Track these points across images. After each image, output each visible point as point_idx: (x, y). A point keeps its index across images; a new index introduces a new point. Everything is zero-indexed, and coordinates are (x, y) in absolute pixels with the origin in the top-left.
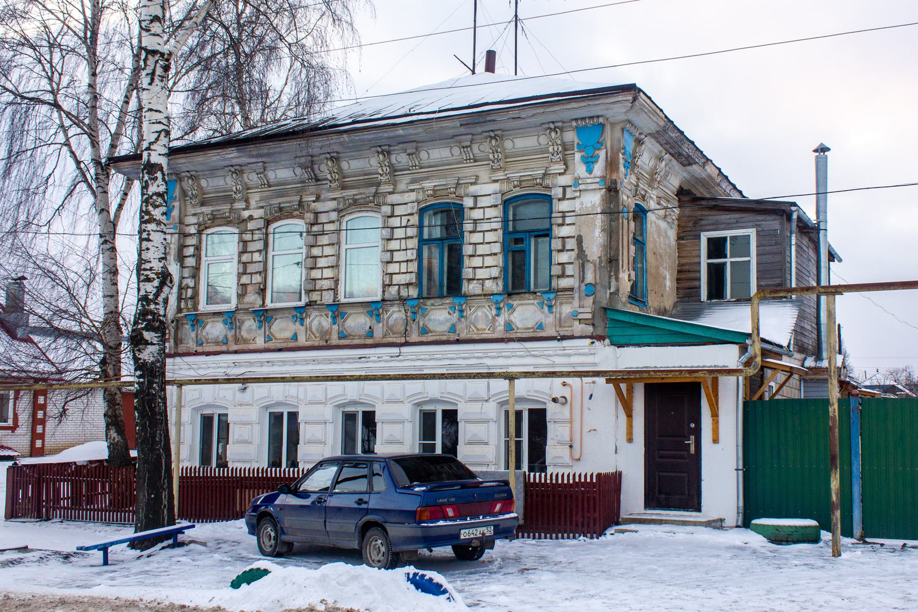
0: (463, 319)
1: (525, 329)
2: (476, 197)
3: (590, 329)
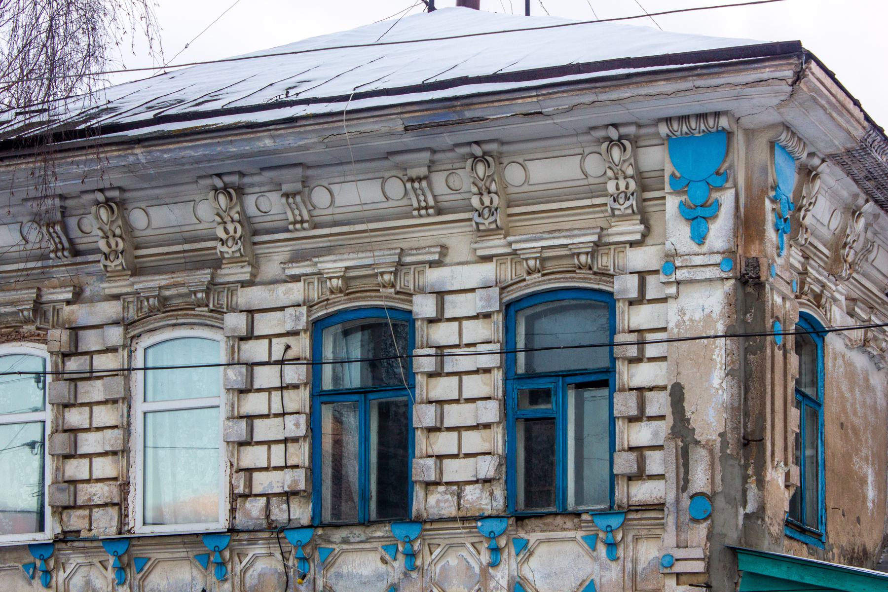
0: (414, 575)
2: (441, 295)
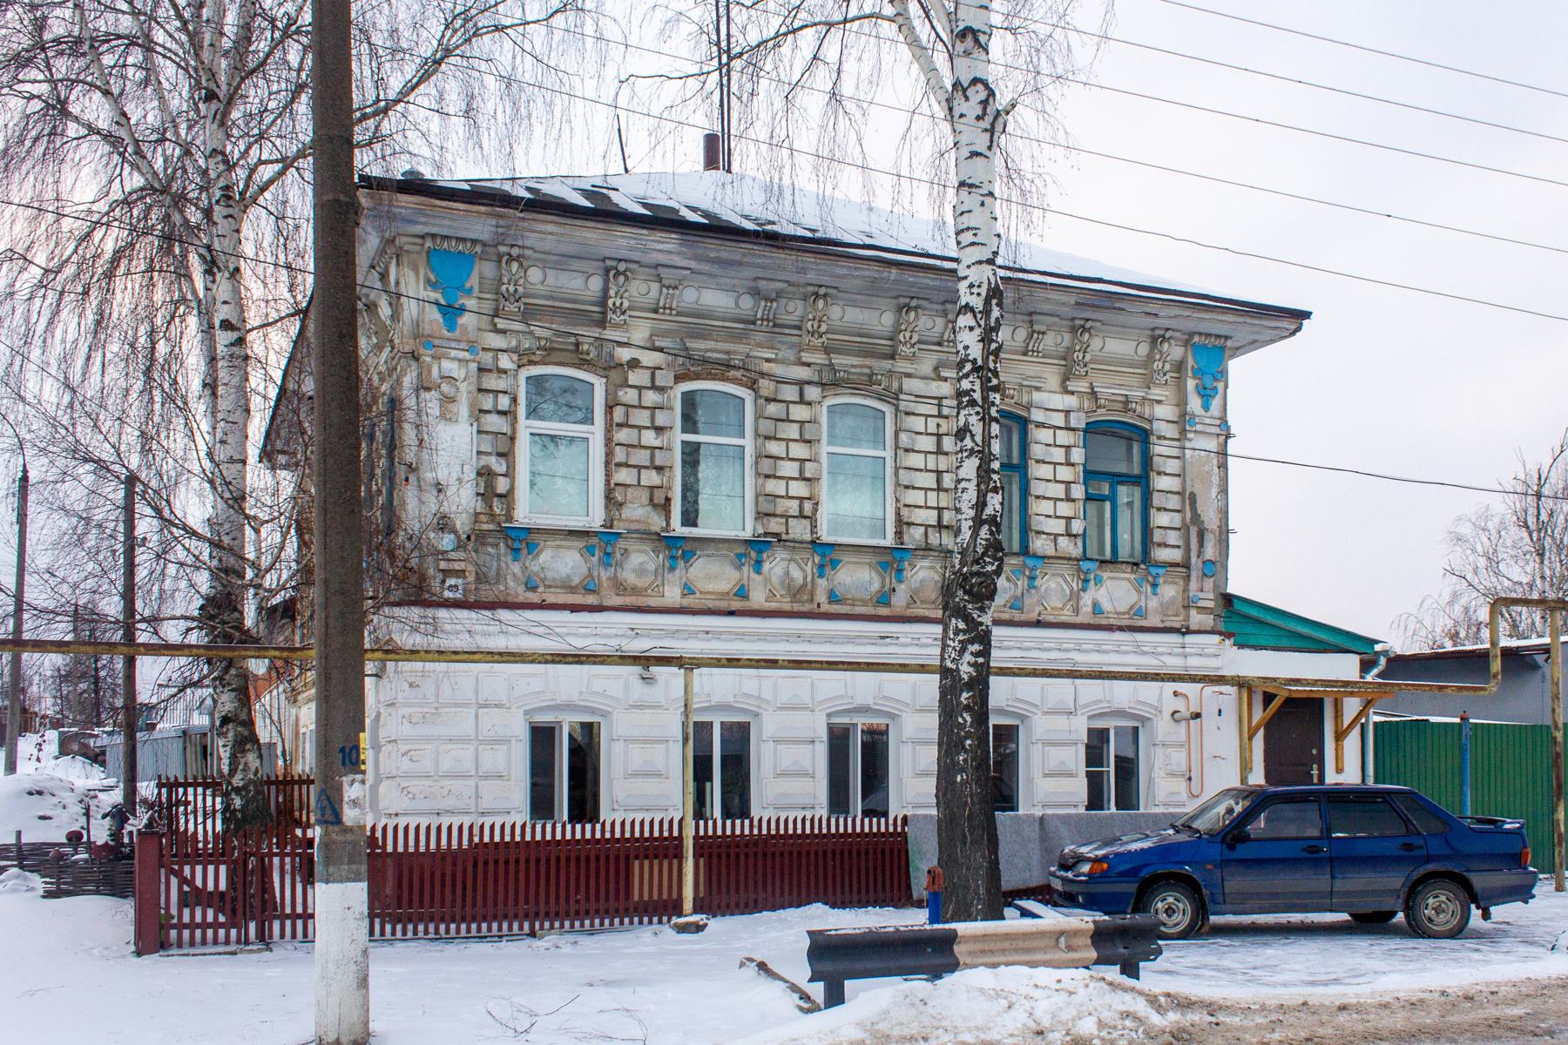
0: (1033, 591)
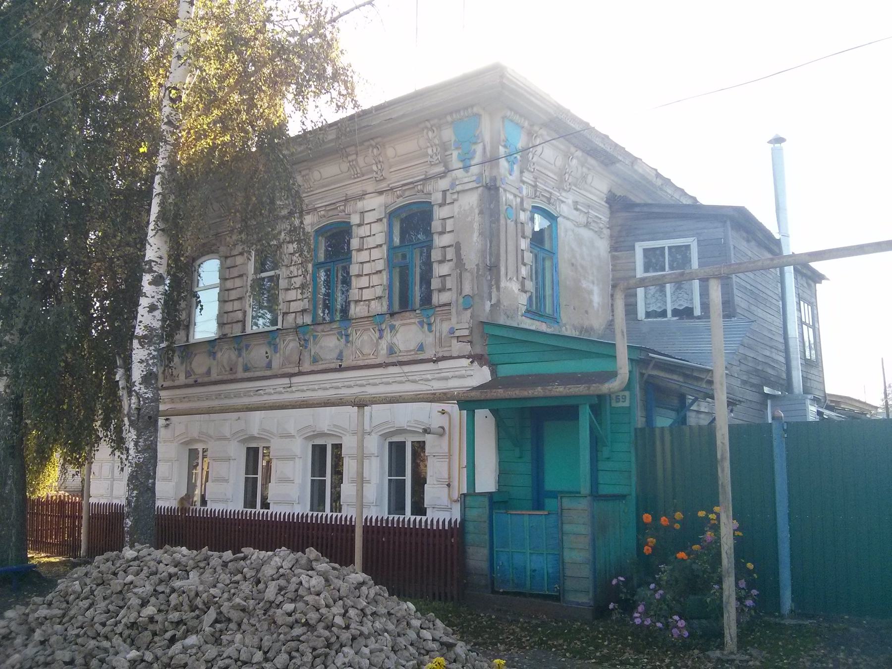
0: (349, 345)
1: (407, 351)
2: (362, 213)
3: (467, 348)
